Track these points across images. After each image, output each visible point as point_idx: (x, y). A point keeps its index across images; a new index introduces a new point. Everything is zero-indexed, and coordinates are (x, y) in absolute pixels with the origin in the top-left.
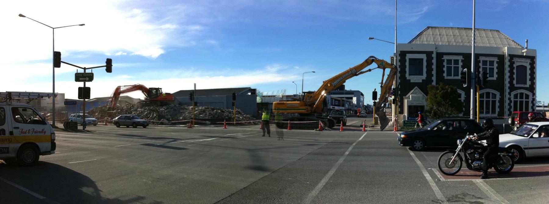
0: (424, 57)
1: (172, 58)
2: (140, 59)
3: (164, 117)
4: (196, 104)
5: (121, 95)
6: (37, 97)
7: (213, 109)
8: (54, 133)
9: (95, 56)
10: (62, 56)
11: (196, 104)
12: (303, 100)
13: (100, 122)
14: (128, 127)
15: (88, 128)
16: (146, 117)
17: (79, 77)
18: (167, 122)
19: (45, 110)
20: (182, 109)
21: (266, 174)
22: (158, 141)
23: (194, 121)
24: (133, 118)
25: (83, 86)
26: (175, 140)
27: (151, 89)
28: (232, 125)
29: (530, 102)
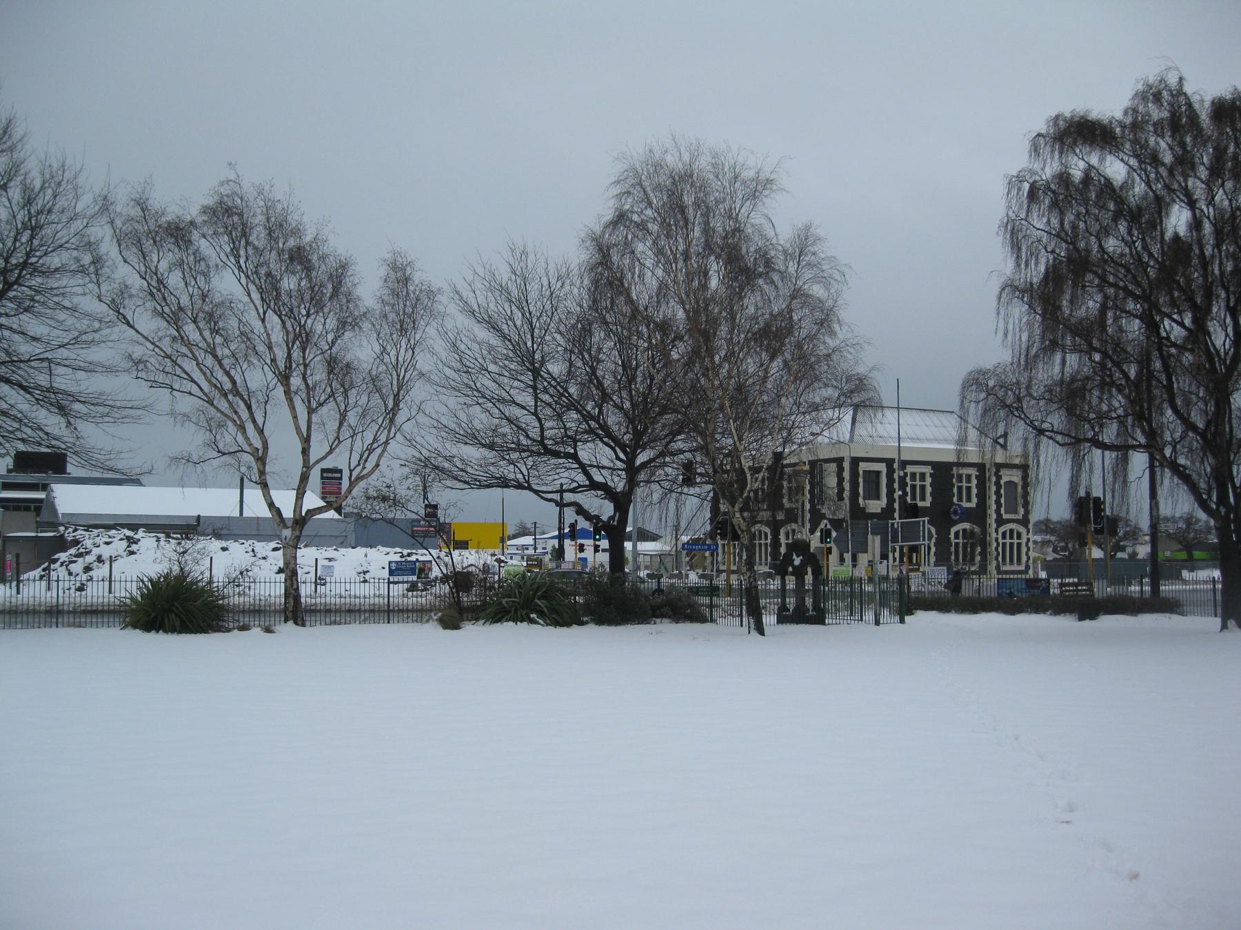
0: (882, 467)
29: (1024, 545)
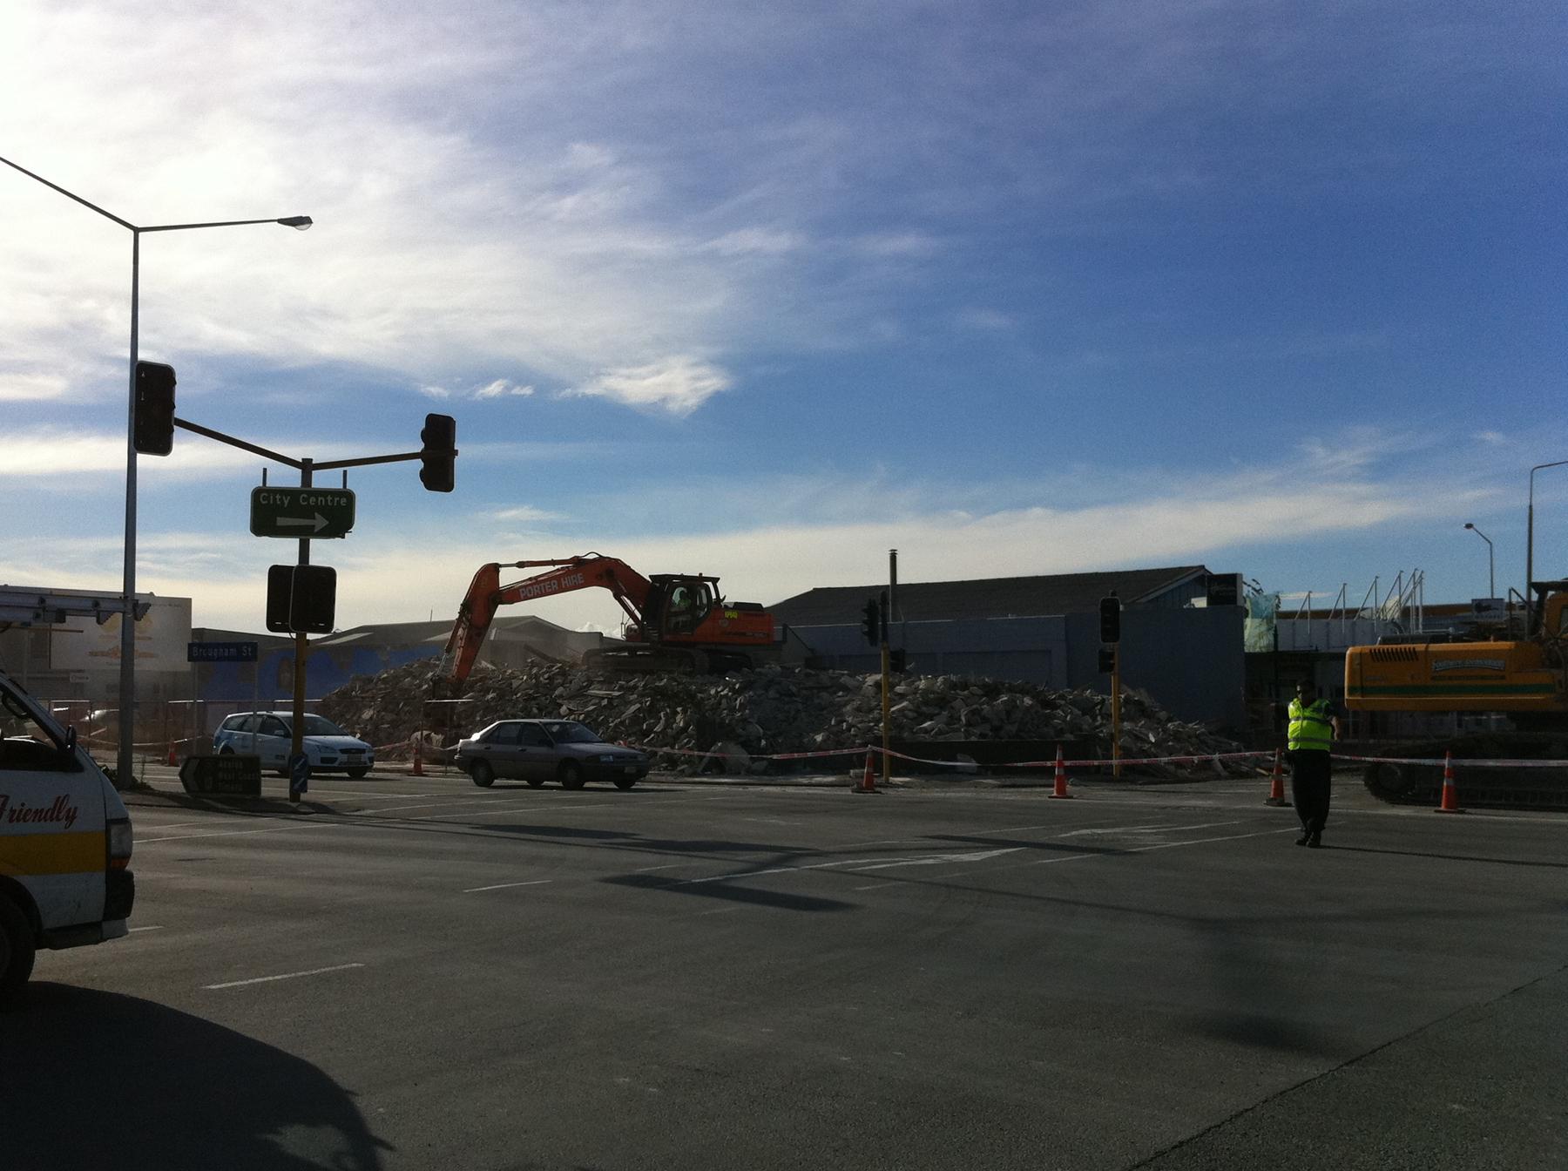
1: (773, 418)
2: (613, 419)
3: (727, 733)
4: (897, 663)
5: (503, 611)
6: (28, 616)
7: (992, 692)
8: (125, 822)
9: (347, 391)
10: (180, 392)
11: (897, 663)
12: (1535, 626)
13: (386, 757)
14: (535, 784)
15: (317, 791)
16: (635, 729)
17: (272, 512)
18: (744, 756)
19: (78, 690)
20: (825, 688)
21: (1309, 1069)
22: (695, 863)
23: (886, 751)
24: (565, 735)
25: (293, 561)
26: (788, 856)
27: (664, 583)
28: (1101, 776)
